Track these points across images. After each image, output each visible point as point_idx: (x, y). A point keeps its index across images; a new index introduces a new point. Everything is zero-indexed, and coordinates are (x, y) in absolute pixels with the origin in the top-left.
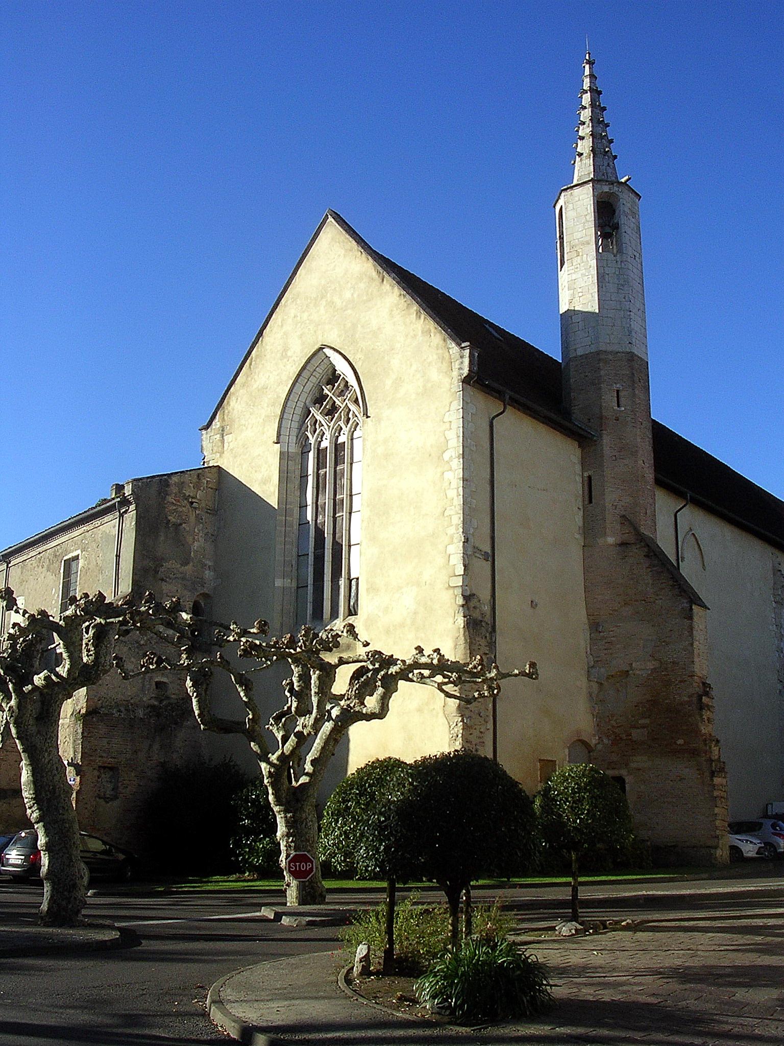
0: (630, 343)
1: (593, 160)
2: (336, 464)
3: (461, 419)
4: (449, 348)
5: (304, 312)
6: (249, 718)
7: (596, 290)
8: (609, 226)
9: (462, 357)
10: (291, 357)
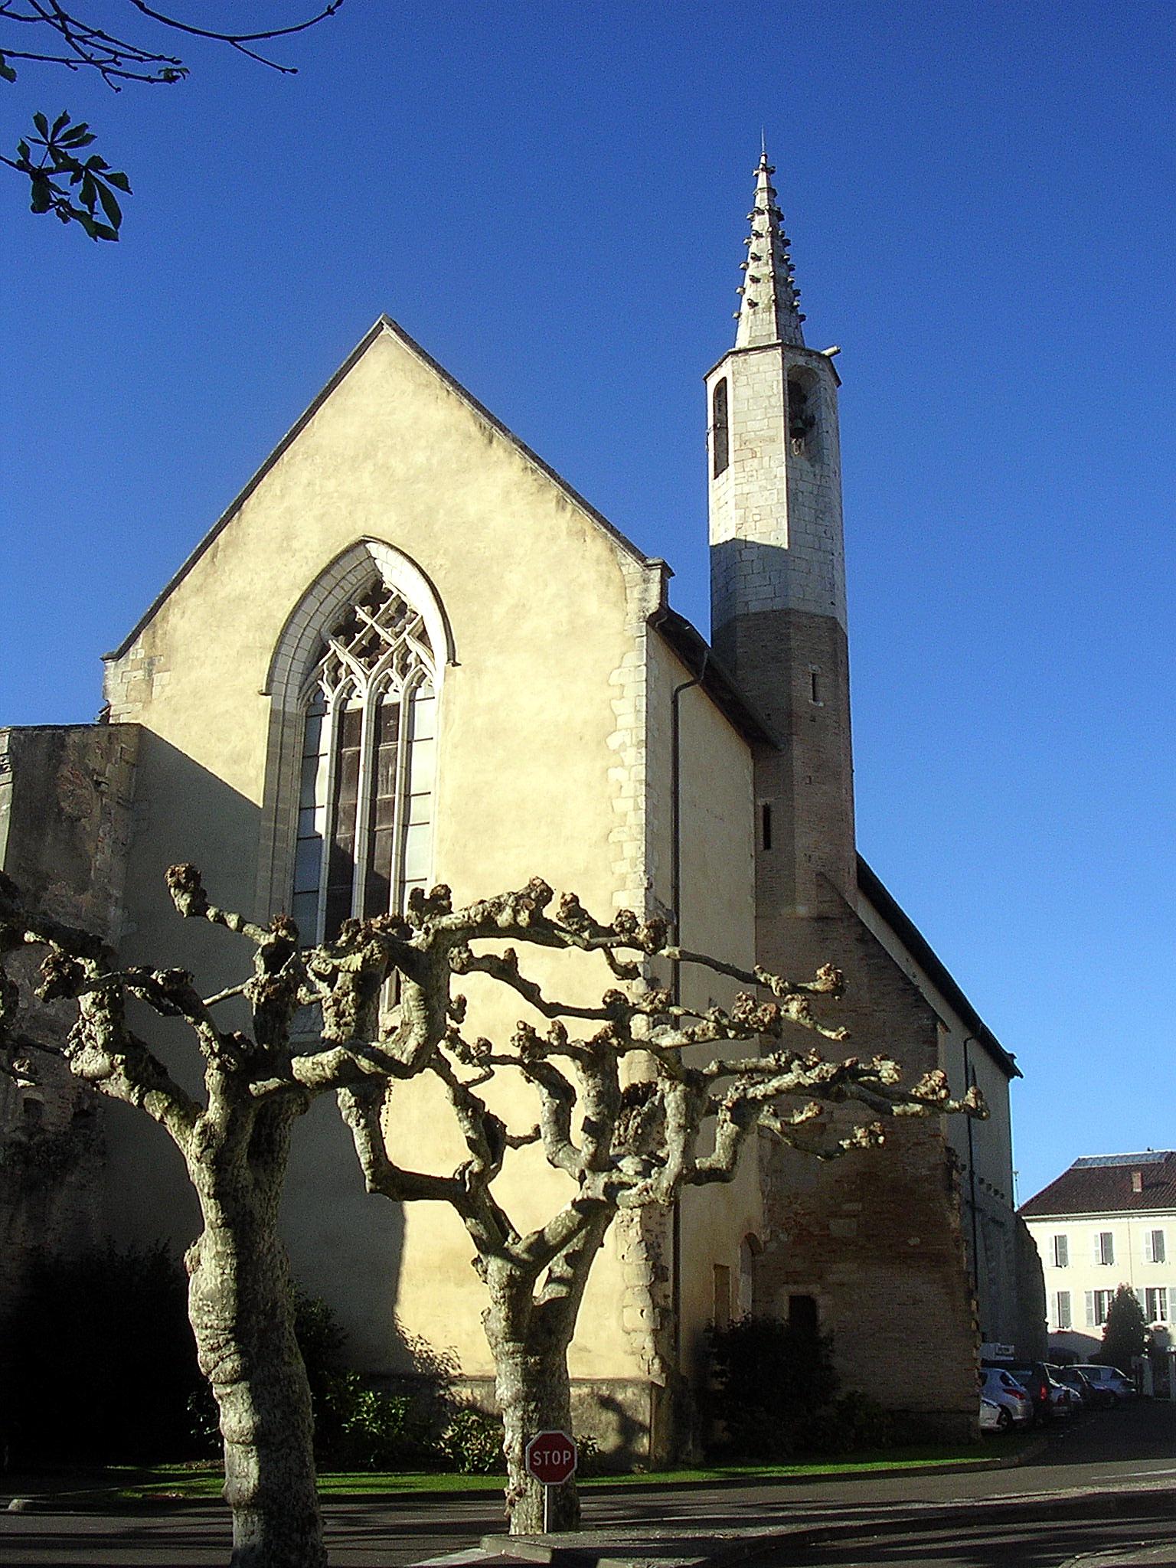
0: (832, 603)
1: (776, 315)
2: (378, 740)
3: (644, 684)
4: (620, 565)
5: (329, 478)
6: (470, 1172)
7: (785, 514)
8: (801, 418)
9: (646, 581)
10: (301, 550)
